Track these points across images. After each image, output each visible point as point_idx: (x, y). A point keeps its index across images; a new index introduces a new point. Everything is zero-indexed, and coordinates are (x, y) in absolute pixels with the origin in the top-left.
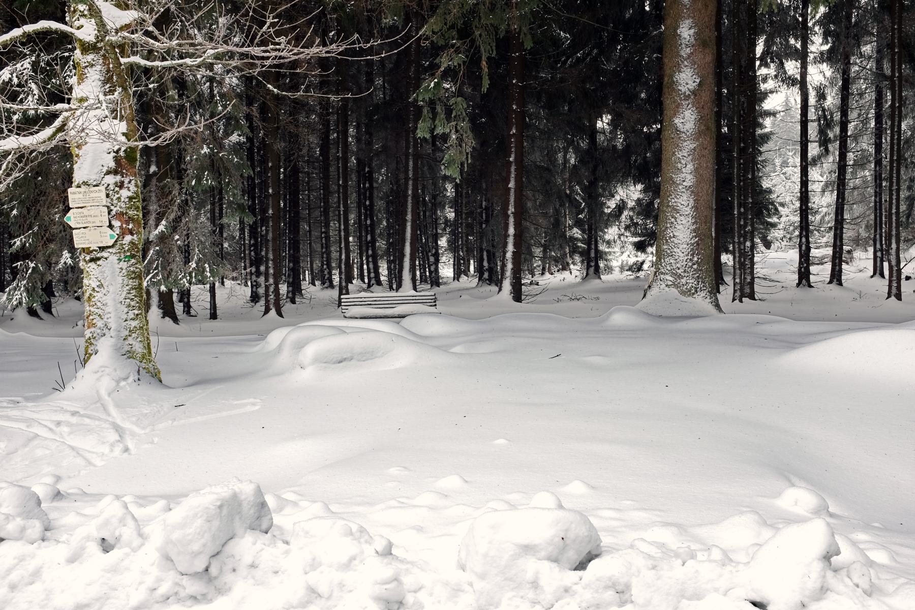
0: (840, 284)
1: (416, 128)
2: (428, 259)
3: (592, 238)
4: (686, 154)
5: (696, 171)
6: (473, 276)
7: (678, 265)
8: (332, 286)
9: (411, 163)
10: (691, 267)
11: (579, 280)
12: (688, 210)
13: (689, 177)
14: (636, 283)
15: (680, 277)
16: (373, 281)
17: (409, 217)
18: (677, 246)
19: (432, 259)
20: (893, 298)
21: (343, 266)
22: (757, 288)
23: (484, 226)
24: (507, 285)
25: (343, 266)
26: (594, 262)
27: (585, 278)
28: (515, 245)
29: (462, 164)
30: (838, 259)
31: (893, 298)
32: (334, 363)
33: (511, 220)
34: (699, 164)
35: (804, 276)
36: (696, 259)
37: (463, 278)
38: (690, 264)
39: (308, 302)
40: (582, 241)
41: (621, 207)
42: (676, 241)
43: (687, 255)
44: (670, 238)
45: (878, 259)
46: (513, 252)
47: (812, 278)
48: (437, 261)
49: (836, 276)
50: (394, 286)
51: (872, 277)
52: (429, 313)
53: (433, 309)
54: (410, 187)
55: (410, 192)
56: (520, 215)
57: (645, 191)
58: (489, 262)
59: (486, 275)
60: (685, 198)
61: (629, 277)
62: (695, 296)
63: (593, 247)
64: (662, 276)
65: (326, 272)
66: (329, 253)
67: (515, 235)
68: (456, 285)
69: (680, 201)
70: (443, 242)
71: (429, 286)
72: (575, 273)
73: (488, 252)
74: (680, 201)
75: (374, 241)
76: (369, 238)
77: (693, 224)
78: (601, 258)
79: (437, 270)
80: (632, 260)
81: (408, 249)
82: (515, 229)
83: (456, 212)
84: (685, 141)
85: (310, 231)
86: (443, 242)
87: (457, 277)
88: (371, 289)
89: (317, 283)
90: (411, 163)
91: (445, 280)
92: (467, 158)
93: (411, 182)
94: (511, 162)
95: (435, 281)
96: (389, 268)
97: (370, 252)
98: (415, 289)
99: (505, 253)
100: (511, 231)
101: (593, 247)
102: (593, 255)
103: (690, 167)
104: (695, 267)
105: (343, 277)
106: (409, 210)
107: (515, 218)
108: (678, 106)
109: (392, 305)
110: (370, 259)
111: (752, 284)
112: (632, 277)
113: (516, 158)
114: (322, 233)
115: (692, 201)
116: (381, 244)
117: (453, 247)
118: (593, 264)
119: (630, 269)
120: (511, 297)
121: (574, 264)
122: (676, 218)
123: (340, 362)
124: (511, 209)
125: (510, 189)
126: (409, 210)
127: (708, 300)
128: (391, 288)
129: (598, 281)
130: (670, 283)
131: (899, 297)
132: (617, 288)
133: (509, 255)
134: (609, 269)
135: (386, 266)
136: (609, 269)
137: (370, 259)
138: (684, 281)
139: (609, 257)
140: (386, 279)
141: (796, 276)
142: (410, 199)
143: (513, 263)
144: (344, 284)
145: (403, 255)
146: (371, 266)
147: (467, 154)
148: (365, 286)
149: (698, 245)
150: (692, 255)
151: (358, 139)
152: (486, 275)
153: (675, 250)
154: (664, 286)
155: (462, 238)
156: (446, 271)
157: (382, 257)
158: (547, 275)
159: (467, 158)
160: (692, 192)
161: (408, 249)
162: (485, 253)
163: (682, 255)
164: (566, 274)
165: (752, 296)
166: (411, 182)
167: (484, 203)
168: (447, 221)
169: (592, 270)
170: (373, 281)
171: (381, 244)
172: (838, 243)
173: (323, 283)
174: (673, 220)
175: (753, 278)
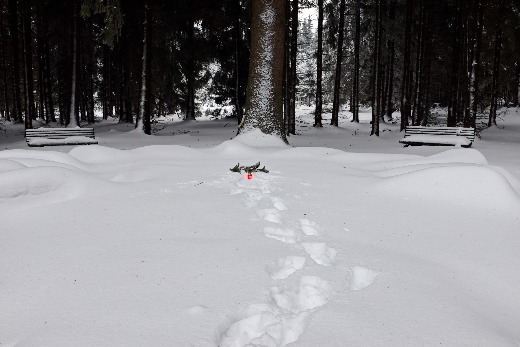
0: (337, 125)
1: (80, 9)
2: (87, 106)
3: (191, 96)
4: (267, 39)
5: (273, 51)
6: (115, 116)
8: (21, 122)
9: (75, 41)
10: (270, 114)
11: (181, 120)
12: (268, 77)
13: (269, 54)
15: (262, 120)
16: (50, 119)
17: (74, 77)
18: (260, 100)
19: (89, 105)
20: (375, 135)
21: (28, 109)
23: (123, 85)
24: (141, 124)
25: (28, 109)
26: (190, 111)
27: (186, 119)
28: (146, 98)
29: (115, 37)
30: (335, 112)
31: (375, 135)
32: (10, 197)
33: (144, 81)
34: (275, 46)
36: (272, 109)
37: (109, 118)
38: (269, 112)
39: (4, 132)
40: (182, 96)
41: (208, 76)
43: (267, 106)
44: (256, 94)
46: (145, 102)
48: (92, 107)
49: (335, 121)
50: (64, 122)
51: (352, 121)
52: (89, 144)
53: (91, 140)
54: (75, 57)
55: (75, 61)
56: (149, 78)
57: (222, 67)
58: (126, 108)
59: (124, 116)
60: (266, 68)
61: (212, 119)
64: (251, 120)
65: (17, 113)
66: (19, 100)
67: (146, 91)
68: (104, 122)
69: (263, 70)
70: (96, 95)
71: (87, 123)
73: (126, 101)
74: (263, 70)
75: (50, 93)
76: (47, 91)
77: (271, 85)
79: (92, 113)
81: (73, 99)
82: (146, 87)
83: (103, 77)
84: (267, 30)
85: (6, 85)
86: (96, 95)
87: (105, 117)
88: (49, 124)
89: (12, 119)
90: (75, 41)
92: (119, 32)
93: (75, 54)
94: (144, 43)
95: (92, 119)
96: (60, 111)
97: (48, 100)
98: (78, 125)
99: (139, 102)
100: (144, 88)
102: (190, 105)
103: (270, 47)
104: (272, 114)
105: (28, 116)
106: (74, 72)
107: (146, 80)
108: (263, 6)
109: (63, 137)
110: (48, 105)
111: (293, 124)
112: (214, 119)
113: (147, 40)
114: (14, 86)
115: (271, 70)
116: (55, 95)
117: (101, 99)
118: (190, 110)
120: (143, 131)
122: (260, 82)
123: (15, 196)
124: (144, 74)
125: (143, 60)
126: (74, 72)
127: (280, 136)
128: (62, 124)
129: (193, 121)
131: (378, 134)
132: (206, 125)
133: (142, 103)
134: (200, 114)
135: (58, 109)
136: (200, 114)
138: (265, 123)
139: (198, 107)
140: (58, 117)
141: (314, 120)
142: (74, 65)
143: (145, 109)
144: (29, 121)
145: (70, 103)
146: (49, 109)
147: (119, 30)
148: (44, 122)
149: (274, 99)
150: (270, 106)
151: (37, 25)
152: (124, 116)
153: (259, 102)
154: (251, 126)
155: (108, 93)
156: (98, 113)
157: (56, 104)
159: (119, 32)
160: (271, 64)
161: (73, 99)
162: (124, 102)
163: (264, 106)
165: (294, 133)
166: (75, 54)
167: (123, 71)
168: (98, 81)
169: (190, 114)
171: (55, 95)
172: (336, 102)
173: (15, 120)
174: (258, 82)
175: (294, 121)
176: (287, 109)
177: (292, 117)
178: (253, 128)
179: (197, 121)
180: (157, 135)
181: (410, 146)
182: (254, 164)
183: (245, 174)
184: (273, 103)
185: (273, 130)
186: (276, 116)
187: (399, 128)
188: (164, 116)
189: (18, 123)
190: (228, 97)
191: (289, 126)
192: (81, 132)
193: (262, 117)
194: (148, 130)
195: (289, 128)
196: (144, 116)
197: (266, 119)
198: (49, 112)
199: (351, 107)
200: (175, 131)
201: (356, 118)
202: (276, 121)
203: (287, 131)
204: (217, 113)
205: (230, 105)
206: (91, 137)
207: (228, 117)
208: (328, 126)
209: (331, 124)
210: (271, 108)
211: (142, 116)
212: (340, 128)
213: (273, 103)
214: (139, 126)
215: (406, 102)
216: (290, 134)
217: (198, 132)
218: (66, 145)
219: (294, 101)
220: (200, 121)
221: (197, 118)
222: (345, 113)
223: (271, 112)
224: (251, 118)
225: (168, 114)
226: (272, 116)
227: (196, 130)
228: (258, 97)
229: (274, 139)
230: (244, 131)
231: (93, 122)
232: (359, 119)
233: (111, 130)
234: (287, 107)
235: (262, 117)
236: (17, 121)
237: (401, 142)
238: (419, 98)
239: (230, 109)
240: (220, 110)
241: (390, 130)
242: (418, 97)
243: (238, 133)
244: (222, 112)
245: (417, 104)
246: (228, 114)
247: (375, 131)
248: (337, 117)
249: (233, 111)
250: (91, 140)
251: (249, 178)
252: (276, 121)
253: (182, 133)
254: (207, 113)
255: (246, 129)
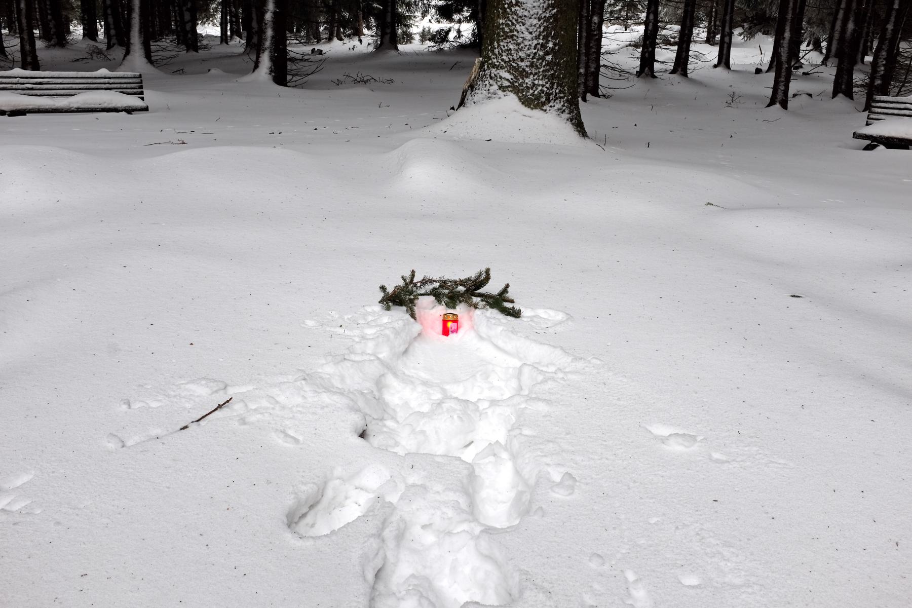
0: (685, 74)
7: (522, 54)
10: (543, 58)
11: (371, 49)
14: (439, 58)
15: (524, 74)
18: (521, 20)
20: (778, 106)
22: (602, 81)
24: (265, 60)
26: (391, 32)
27: (379, 48)
30: (684, 43)
31: (778, 106)
35: (648, 61)
36: (551, 45)
38: (541, 53)
42: (520, 12)
43: (537, 38)
45: (726, 45)
46: (275, 13)
47: (657, 66)
49: (681, 65)
51: (715, 66)
52: (129, 111)
53: (133, 101)
61: (430, 49)
62: (546, 107)
63: (389, 9)
64: (494, 71)
72: (366, 40)
78: (399, 22)
80: (435, 27)
91: (205, 42)
95: (192, 41)
99: (263, 13)
101: (389, 9)
102: (389, 19)
104: (549, 58)
110: (109, 11)
111: (596, 74)
112: (435, 49)
118: (388, 31)
119: (433, 38)
120: (270, 77)
121: (369, 28)
127: (566, 116)
129: (393, 52)
130: (506, 84)
131: (784, 105)
132: (418, 64)
133: (268, 16)
134: (408, 38)
136: (408, 38)
137: (109, 11)
143: (274, 29)
149: (556, 20)
150: (546, 38)
153: (518, 27)
154: (495, 87)
158: (336, 41)
163: (529, 37)
164: (355, 42)
165: (595, 94)
169: (387, 37)
170: (114, 41)
175: (598, 67)
176: (584, 41)
177: (593, 57)
178: (500, 93)
179: (401, 54)
180: (301, 86)
181: (882, 147)
182: (470, 272)
183: (431, 310)
184: (553, 28)
185: (548, 100)
186: (558, 64)
187: (830, 88)
188: (341, 39)
189: (54, 46)
190: (465, 5)
191: (586, 80)
192: (112, 81)
193: (522, 64)
194: (280, 76)
195: (585, 84)
196: (272, 44)
197: (534, 71)
198: (112, 26)
199: (709, 33)
200: (342, 78)
201: (724, 60)
202: (558, 77)
203: (581, 89)
204: (441, 36)
205: (469, 22)
206: (135, 94)
207: (462, 47)
208: (667, 75)
209: (673, 72)
210: (547, 42)
211: (268, 44)
212: (694, 81)
213: (553, 28)
214: (260, 65)
215: (854, 30)
216: (589, 96)
217: (392, 81)
218: (73, 111)
219: (601, 22)
220: (406, 54)
221: (401, 47)
222: (704, 53)
223: (547, 54)
224: (494, 66)
225: (349, 36)
226: (548, 64)
227: (387, 76)
228: (515, 13)
229: (550, 124)
230: (476, 99)
231: (196, 49)
232: (731, 62)
233: (213, 71)
234: (584, 34)
235: (522, 64)
236: (52, 42)
237: (856, 136)
238: (896, 24)
239: (468, 29)
240: (449, 30)
241: (810, 95)
242: (893, 19)
243: (462, 103)
244: (452, 36)
245: (889, 35)
246: (463, 40)
247: (780, 97)
248: (687, 56)
249: (474, 35)
250: (133, 101)
251: (446, 332)
252: (558, 77)
253: (356, 82)
254: (424, 36)
255: (480, 94)
